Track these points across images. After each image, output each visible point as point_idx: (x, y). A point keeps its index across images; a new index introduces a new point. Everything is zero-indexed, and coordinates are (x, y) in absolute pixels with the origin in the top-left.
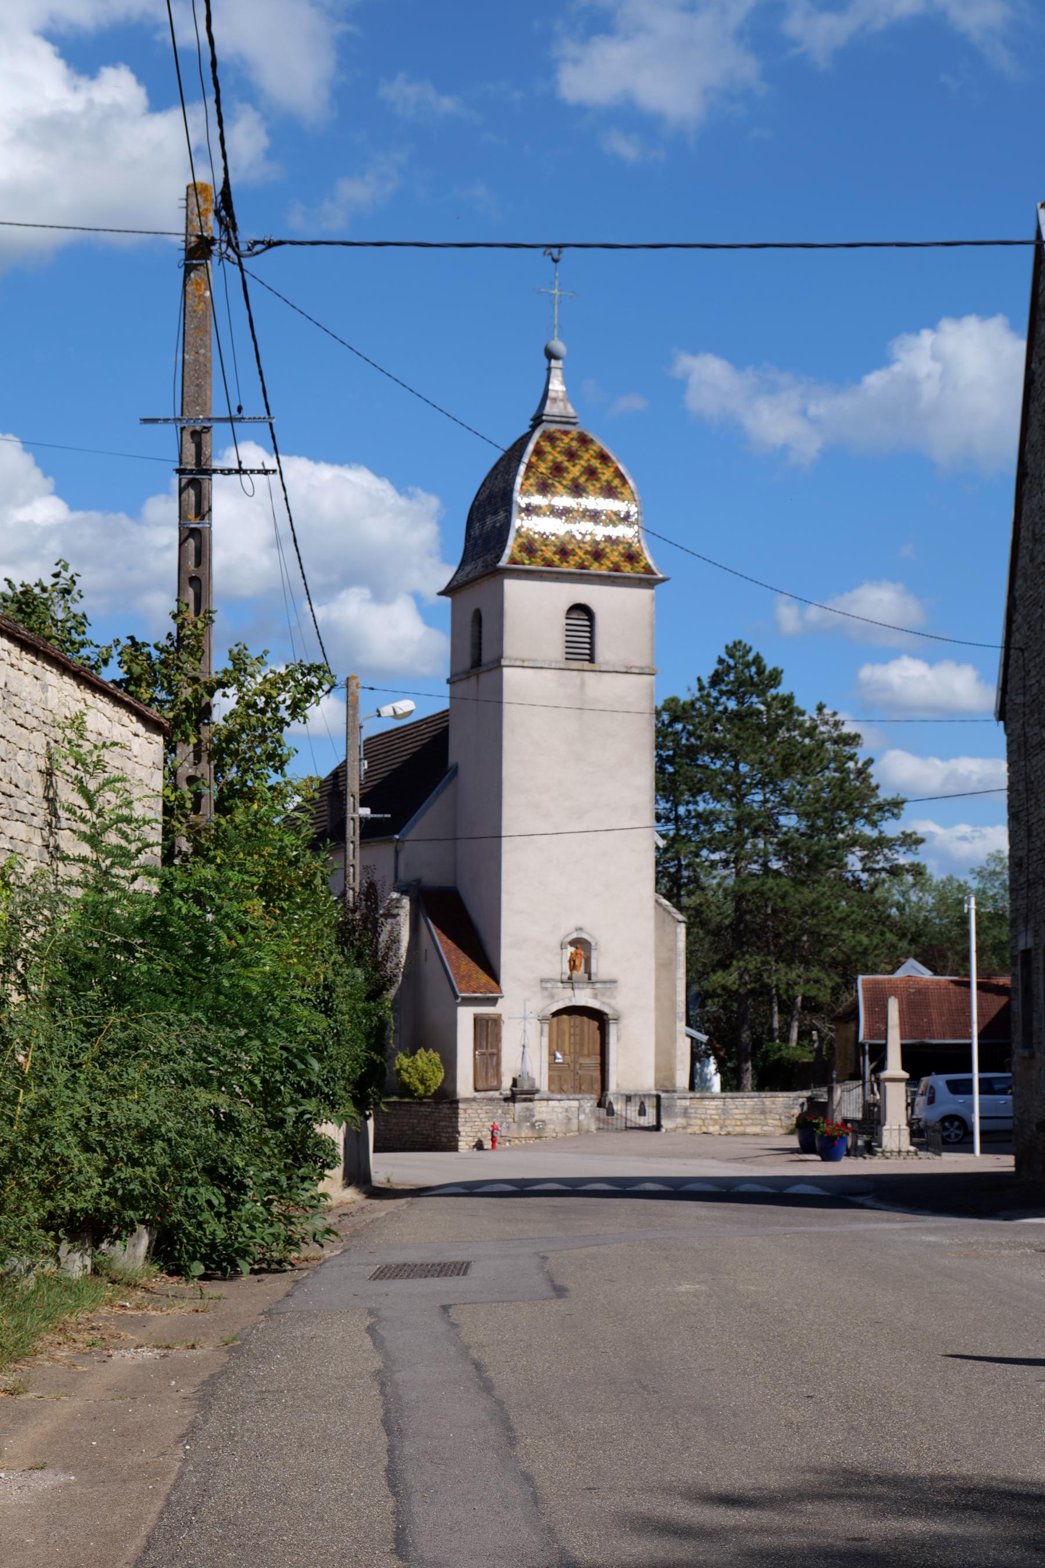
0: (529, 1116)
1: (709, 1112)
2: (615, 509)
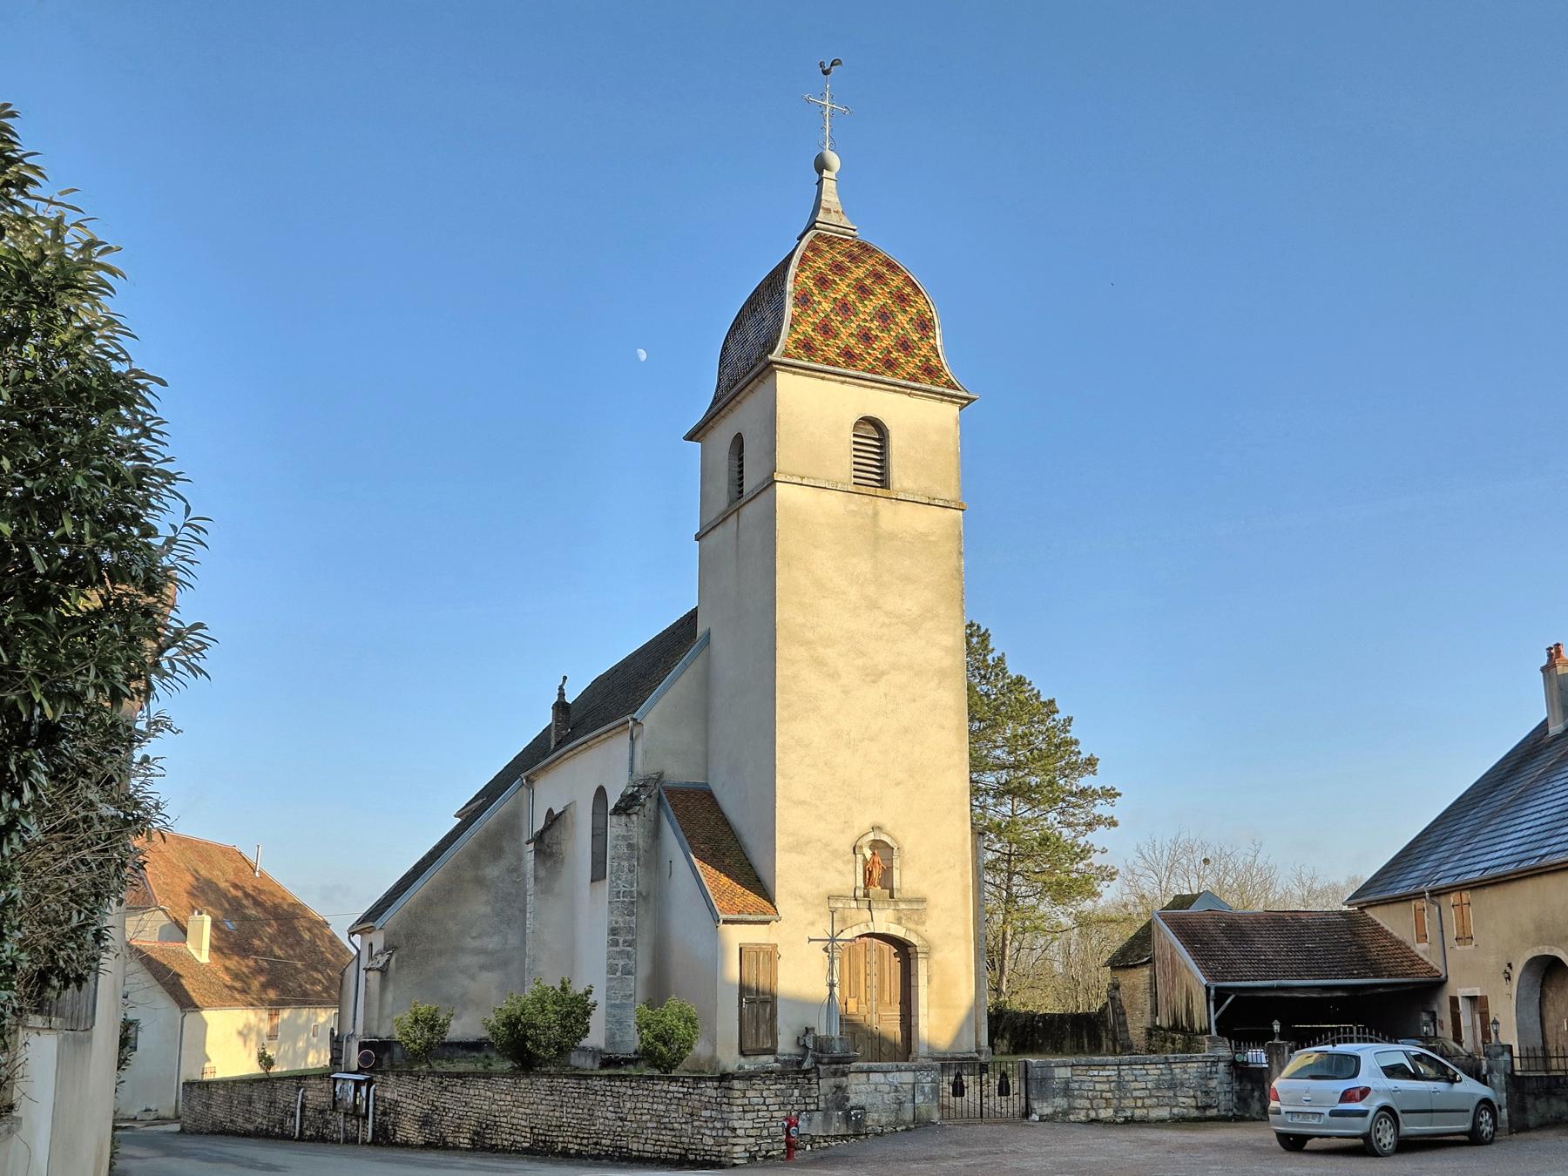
0: (840, 1098)
1: (1098, 1087)
2: (605, 937)
